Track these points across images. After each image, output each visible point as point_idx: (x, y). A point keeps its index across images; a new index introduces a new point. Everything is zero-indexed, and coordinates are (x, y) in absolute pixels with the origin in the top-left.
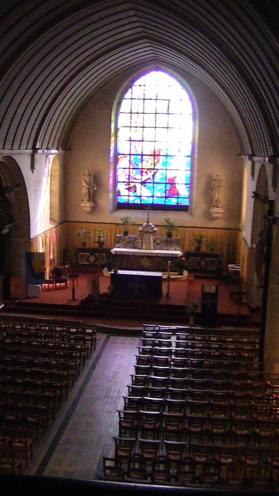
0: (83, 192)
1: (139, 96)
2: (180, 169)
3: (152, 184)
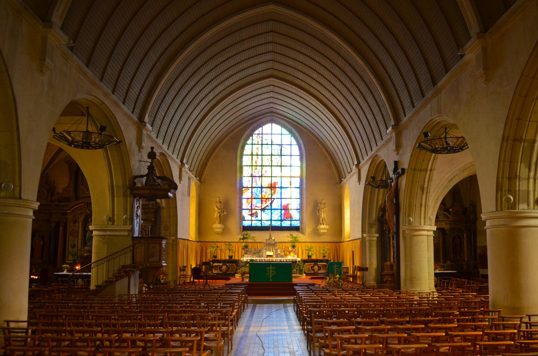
2: (291, 196)
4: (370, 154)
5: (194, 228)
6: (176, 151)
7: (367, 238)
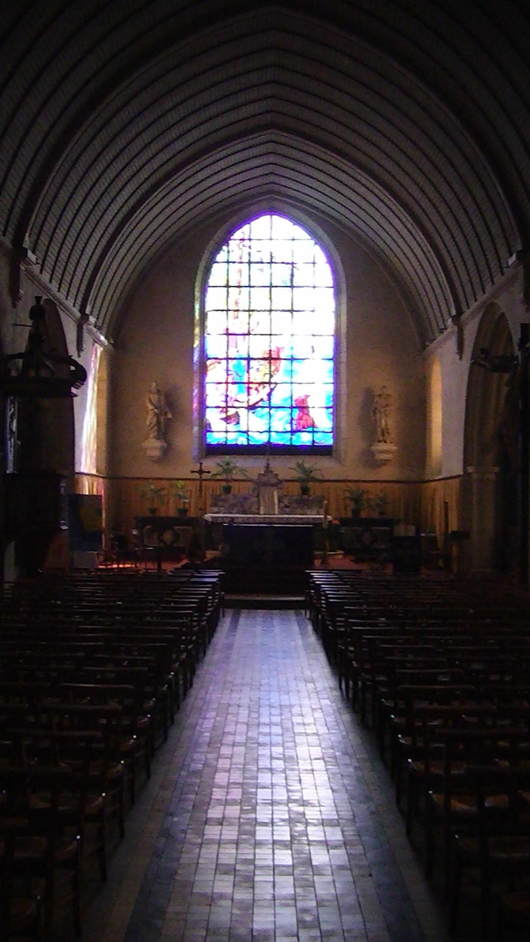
0: (148, 422)
1: (241, 258)
2: (313, 381)
3: (267, 409)
4: (481, 298)
5: (93, 446)
6: (73, 291)
7: (475, 476)
